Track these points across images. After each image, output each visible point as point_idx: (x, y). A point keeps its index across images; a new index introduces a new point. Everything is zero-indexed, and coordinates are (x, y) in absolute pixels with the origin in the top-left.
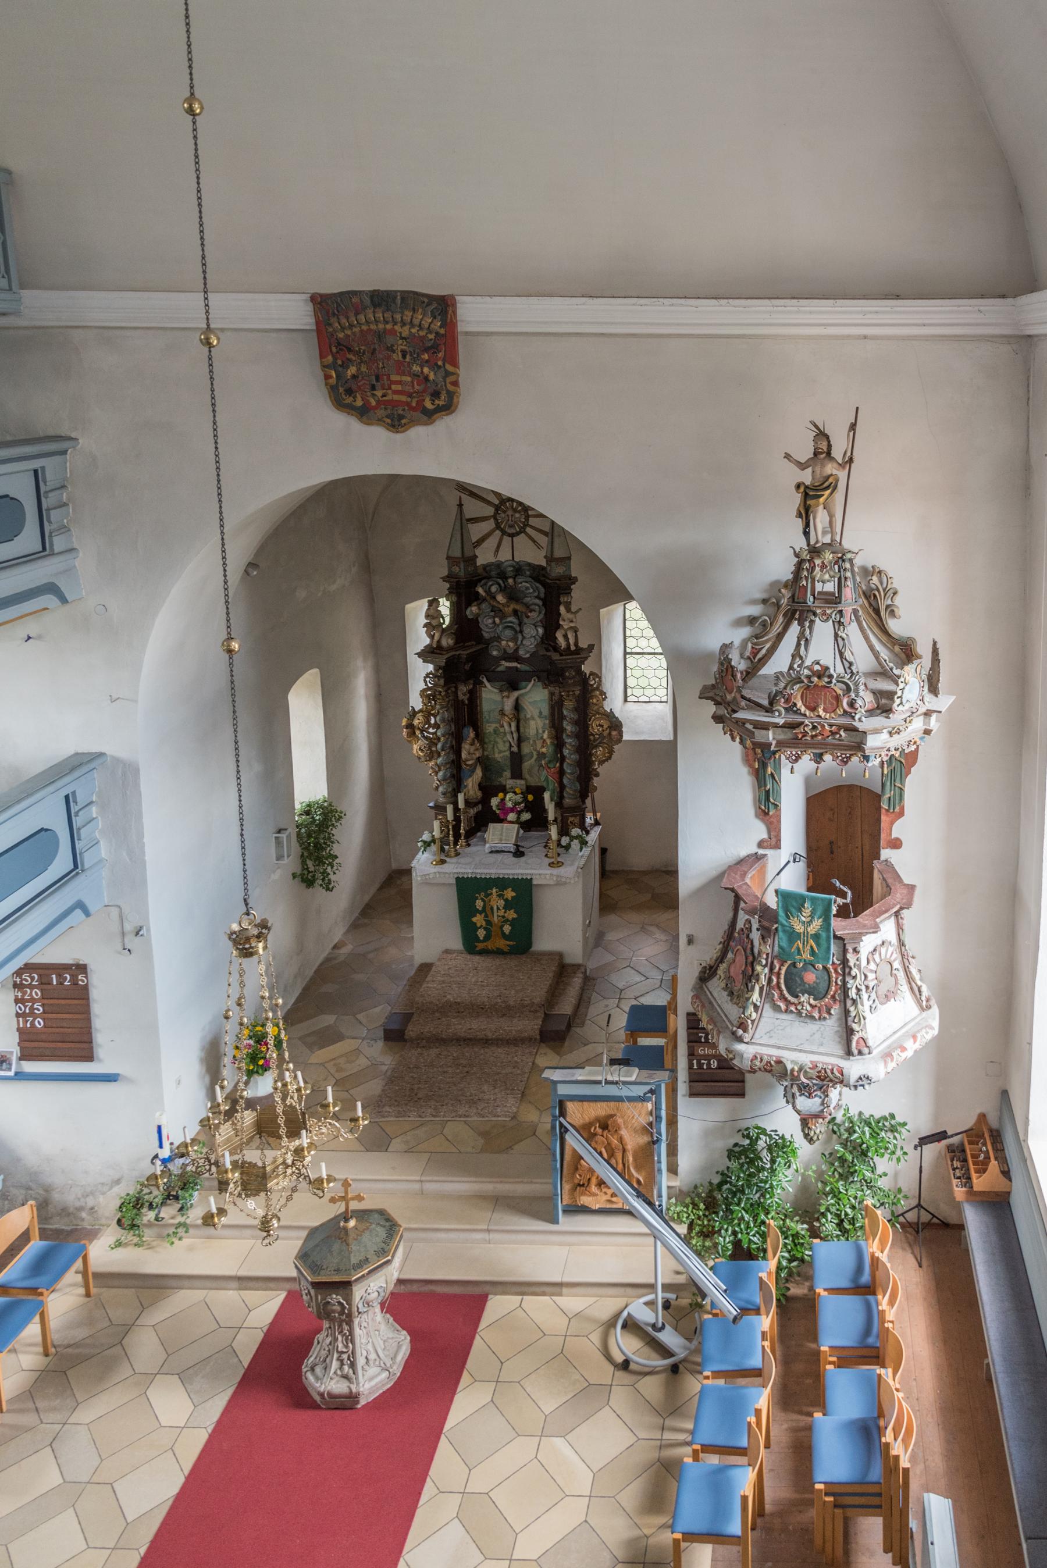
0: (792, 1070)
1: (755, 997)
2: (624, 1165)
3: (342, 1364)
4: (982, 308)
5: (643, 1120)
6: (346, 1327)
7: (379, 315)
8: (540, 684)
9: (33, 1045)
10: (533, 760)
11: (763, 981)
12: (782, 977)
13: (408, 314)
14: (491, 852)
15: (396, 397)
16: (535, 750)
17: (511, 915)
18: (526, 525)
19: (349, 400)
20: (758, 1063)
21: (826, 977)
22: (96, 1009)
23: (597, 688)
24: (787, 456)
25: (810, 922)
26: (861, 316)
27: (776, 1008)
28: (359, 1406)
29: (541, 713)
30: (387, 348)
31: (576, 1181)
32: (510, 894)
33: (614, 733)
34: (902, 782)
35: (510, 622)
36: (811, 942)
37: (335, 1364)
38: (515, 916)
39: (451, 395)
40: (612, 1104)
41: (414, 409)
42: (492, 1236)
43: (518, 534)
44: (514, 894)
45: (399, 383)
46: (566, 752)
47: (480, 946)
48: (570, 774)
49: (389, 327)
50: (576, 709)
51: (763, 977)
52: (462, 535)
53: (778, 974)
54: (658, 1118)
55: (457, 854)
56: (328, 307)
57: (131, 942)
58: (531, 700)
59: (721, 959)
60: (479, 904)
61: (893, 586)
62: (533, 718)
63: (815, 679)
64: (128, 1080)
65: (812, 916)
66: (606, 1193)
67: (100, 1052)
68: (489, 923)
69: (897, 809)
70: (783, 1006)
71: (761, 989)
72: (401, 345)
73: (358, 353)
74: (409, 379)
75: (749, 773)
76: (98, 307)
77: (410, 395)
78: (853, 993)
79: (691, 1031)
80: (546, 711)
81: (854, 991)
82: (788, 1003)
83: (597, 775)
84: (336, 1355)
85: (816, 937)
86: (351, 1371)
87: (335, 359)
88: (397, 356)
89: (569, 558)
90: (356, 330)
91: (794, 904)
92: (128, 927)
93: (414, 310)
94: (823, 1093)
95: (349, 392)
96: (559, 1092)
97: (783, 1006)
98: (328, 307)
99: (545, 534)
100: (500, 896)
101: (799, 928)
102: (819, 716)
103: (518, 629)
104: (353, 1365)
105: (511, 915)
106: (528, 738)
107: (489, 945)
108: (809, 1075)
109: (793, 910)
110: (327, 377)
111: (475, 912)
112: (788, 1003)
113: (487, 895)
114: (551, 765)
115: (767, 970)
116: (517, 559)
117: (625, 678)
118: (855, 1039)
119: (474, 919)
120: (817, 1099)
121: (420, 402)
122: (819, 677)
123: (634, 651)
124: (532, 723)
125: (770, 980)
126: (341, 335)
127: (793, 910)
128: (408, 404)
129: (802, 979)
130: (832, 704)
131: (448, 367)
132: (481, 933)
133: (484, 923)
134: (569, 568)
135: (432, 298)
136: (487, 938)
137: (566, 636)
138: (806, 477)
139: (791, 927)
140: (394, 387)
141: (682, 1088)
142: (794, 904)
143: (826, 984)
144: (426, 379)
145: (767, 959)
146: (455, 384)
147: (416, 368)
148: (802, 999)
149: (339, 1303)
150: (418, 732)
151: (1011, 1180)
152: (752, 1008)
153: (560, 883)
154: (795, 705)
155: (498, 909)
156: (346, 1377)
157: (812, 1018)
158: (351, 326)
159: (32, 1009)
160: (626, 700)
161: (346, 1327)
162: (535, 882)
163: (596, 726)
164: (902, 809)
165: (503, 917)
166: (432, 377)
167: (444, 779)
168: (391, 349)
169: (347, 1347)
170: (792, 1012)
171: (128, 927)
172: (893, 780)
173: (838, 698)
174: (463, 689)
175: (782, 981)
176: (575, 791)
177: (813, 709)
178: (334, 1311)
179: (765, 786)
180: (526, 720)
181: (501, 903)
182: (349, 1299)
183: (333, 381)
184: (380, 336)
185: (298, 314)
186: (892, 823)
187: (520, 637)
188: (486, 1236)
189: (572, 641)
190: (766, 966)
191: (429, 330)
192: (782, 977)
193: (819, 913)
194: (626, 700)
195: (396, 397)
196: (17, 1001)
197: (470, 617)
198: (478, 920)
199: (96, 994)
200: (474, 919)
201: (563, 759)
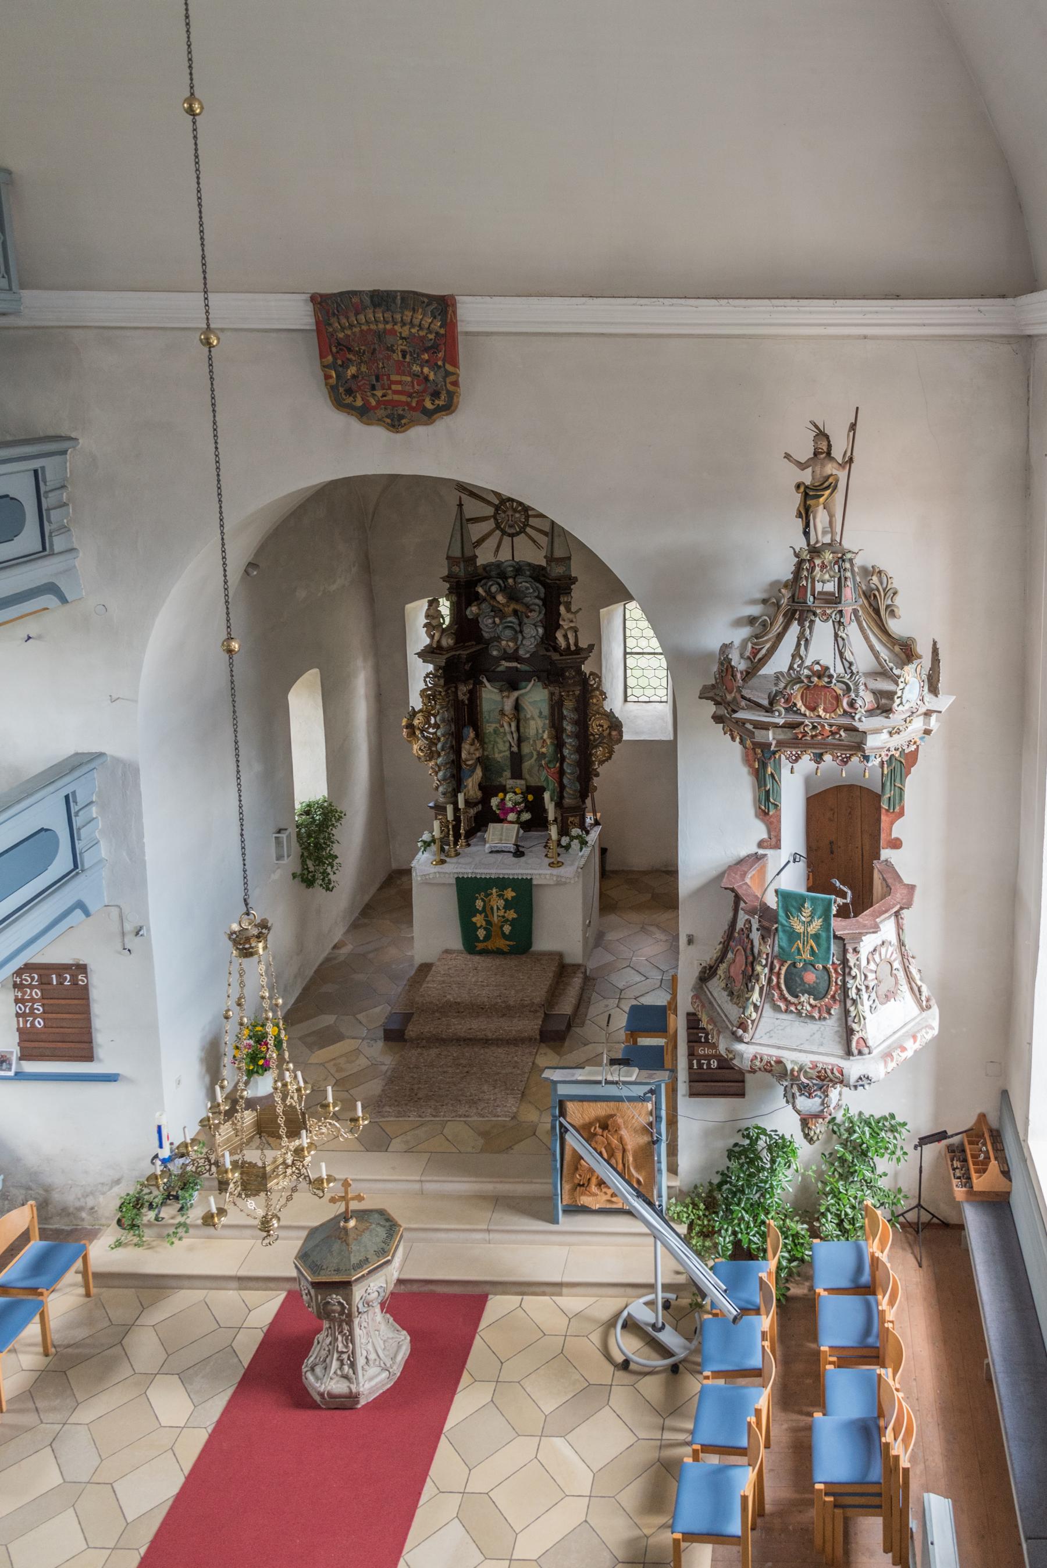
0: (792, 1070)
1: (755, 997)
2: (624, 1165)
3: (342, 1364)
4: (982, 308)
5: (643, 1120)
6: (346, 1327)
7: (379, 315)
8: (540, 684)
9: (33, 1045)
10: (533, 760)
11: (763, 981)
12: (782, 977)
13: (408, 314)
14: (491, 852)
15: (396, 397)
16: (535, 750)
17: (511, 915)
18: (526, 525)
19: (349, 400)
20: (758, 1063)
21: (826, 977)
22: (96, 1009)
23: (597, 688)
24: (787, 456)
25: (810, 922)
27: (776, 1008)
28: (359, 1406)
29: (541, 713)
30: (387, 348)
31: (576, 1181)
32: (510, 894)
34: (902, 782)
35: (510, 622)
36: (811, 942)
37: (335, 1364)
38: (515, 916)
39: (451, 395)
40: (612, 1104)
41: (414, 409)
42: (492, 1236)
43: (518, 534)
44: (514, 894)
45: (399, 383)
46: (566, 752)
47: (480, 946)
48: (570, 774)
49: (389, 327)
50: (576, 709)
51: (763, 977)
52: (462, 535)
53: (778, 974)
54: (658, 1118)
55: (457, 854)
56: (328, 307)
57: (131, 942)
58: (531, 700)
59: (721, 959)
60: (479, 904)
61: (893, 586)
62: (533, 718)
63: (815, 679)
64: (128, 1080)
65: (812, 916)
66: (606, 1193)
67: (100, 1052)
68: (489, 923)
69: (897, 809)
70: (783, 1006)
71: (761, 989)
72: (401, 345)
73: (358, 353)
74: (409, 379)
75: (749, 773)
76: (98, 307)
77: (410, 395)
78: (853, 993)
79: (691, 1031)
80: (546, 711)
81: (854, 991)
82: (788, 1003)
83: (597, 775)
84: (336, 1355)
85: (816, 937)
86: (351, 1371)
87: (335, 359)
88: (397, 356)
89: (569, 558)
90: (356, 330)
91: (794, 904)
92: (128, 927)
93: (414, 310)
94: (823, 1093)
95: (349, 392)
96: (559, 1092)
97: (783, 1006)
98: (328, 307)
99: (545, 534)
100: (500, 896)
101: (799, 928)
102: (819, 716)
103: (518, 629)
104: (353, 1365)
105: (511, 915)
106: (528, 738)
107: (489, 945)
108: (809, 1075)
109: (793, 910)
110: (327, 377)
111: (475, 912)
112: (788, 1003)
113: (487, 895)
114: (551, 765)
115: (767, 970)
116: (517, 559)
117: (625, 678)
118: (855, 1039)
119: (474, 919)
120: (817, 1099)
121: (420, 402)
122: (819, 677)
123: (634, 651)
124: (532, 723)
125: (770, 980)
126: (341, 335)
127: (793, 910)
128: (408, 404)
129: (802, 979)
130: (832, 704)
131: (448, 367)
132: (481, 933)
133: (484, 923)
134: (569, 568)
135: (432, 298)
136: (487, 938)
137: (566, 636)
138: (806, 477)
139: (791, 927)
140: (394, 387)
141: (682, 1088)
142: (794, 904)
143: (826, 984)
144: (426, 379)
146: (455, 384)
147: (416, 368)
148: (802, 999)
149: (339, 1303)
150: (418, 732)
151: (1011, 1180)
152: (752, 1008)
153: (560, 883)
154: (795, 705)
155: (498, 909)
156: (346, 1377)
157: (812, 1018)
158: (351, 326)
159: (32, 1009)
160: (626, 700)
161: (346, 1327)
162: (535, 882)
163: (596, 726)
164: (902, 809)
165: (503, 917)
166: (432, 377)
167: (444, 779)
168: (391, 349)
169: (347, 1347)
170: (792, 1012)
171: (128, 927)
172: (893, 780)
174: (463, 689)
175: (782, 981)
176: (575, 791)
177: (813, 709)
178: (334, 1311)
179: (765, 786)
180: (526, 720)
181: (501, 903)
182: (349, 1299)
183: (333, 381)
184: (380, 336)
185: (298, 314)
186: (892, 823)
187: (520, 637)
188: (486, 1236)
189: (572, 641)
191: (429, 330)
192: (782, 977)
193: (819, 913)
194: (626, 700)
195: (396, 397)
196: (17, 1001)
197: (470, 617)
198: (478, 920)
199: (96, 994)
200: (474, 919)
201: (563, 759)
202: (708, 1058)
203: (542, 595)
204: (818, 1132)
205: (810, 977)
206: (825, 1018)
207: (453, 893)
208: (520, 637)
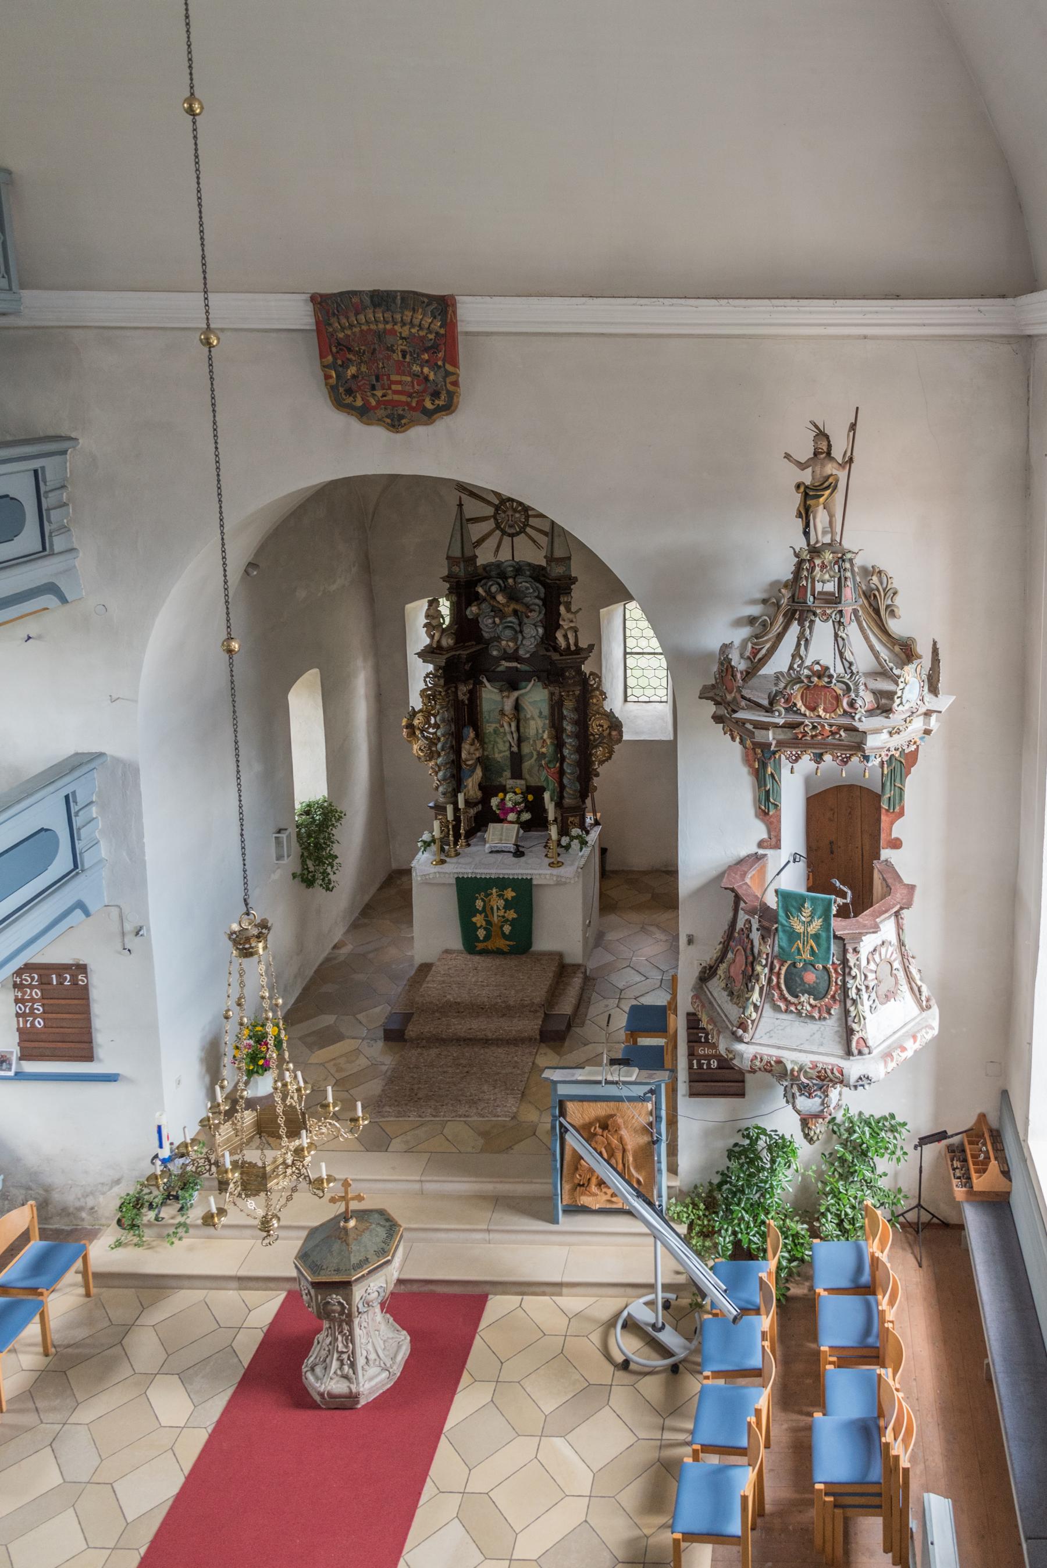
0: (792, 1070)
1: (755, 997)
2: (624, 1165)
3: (342, 1364)
4: (982, 308)
5: (643, 1120)
6: (346, 1327)
7: (379, 315)
9: (33, 1045)
10: (533, 760)
11: (763, 981)
12: (782, 977)
13: (408, 314)
14: (491, 852)
15: (396, 397)
16: (535, 750)
17: (511, 915)
18: (526, 525)
19: (349, 400)
20: (758, 1063)
21: (826, 977)
22: (96, 1009)
23: (597, 688)
24: (787, 456)
25: (810, 922)
26: (861, 316)
28: (359, 1406)
29: (541, 713)
30: (387, 348)
31: (576, 1181)
32: (510, 894)
33: (614, 733)
34: (902, 782)
35: (510, 622)
36: (811, 942)
38: (515, 916)
39: (451, 395)
40: (612, 1104)
41: (414, 409)
42: (492, 1236)
43: (518, 534)
44: (514, 894)
45: (399, 383)
46: (566, 752)
47: (480, 946)
48: (570, 774)
49: (389, 327)
50: (576, 709)
51: (763, 977)
52: (462, 535)
53: (778, 974)
54: (658, 1118)
55: (457, 854)
56: (328, 307)
57: (131, 942)
58: (531, 700)
59: (721, 959)
60: (479, 904)
61: (893, 586)
62: (533, 718)
63: (815, 679)
64: (128, 1080)
65: (812, 916)
66: (606, 1193)
67: (100, 1052)
68: (489, 923)
70: (783, 1006)
71: (761, 989)
72: (401, 345)
73: (358, 353)
74: (409, 379)
75: (749, 773)
76: (98, 307)
77: (410, 395)
78: (853, 993)
79: (691, 1031)
80: (546, 711)
81: (854, 991)
82: (788, 1003)
83: (597, 775)
84: (336, 1355)
85: (816, 937)
86: (351, 1371)
87: (335, 359)
88: (397, 356)
89: (569, 558)
90: (356, 330)
91: (794, 904)
92: (128, 927)
93: (414, 310)
95: (349, 392)
96: (559, 1092)
97: (783, 1006)
98: (328, 307)
99: (545, 534)
100: (500, 896)
101: (799, 928)
103: (518, 629)
104: (353, 1365)
106: (528, 738)
107: (489, 945)
109: (793, 910)
110: (327, 377)
111: (475, 912)
112: (788, 1003)
113: (487, 895)
114: (551, 765)
115: (767, 970)
116: (517, 559)
117: (625, 678)
118: (855, 1039)
119: (474, 919)
120: (817, 1099)
121: (420, 402)
122: (819, 677)
123: (634, 651)
124: (532, 723)
125: (770, 980)
126: (341, 335)
127: (793, 910)
128: (408, 404)
129: (802, 979)
130: (832, 704)
131: (448, 367)
132: (481, 933)
133: (484, 923)
134: (569, 568)
135: (432, 298)
136: (487, 938)
137: (566, 636)
138: (806, 477)
139: (791, 927)
140: (394, 387)
141: (682, 1088)
142: (794, 904)
143: (826, 984)
144: (426, 379)
145: (767, 959)
146: (455, 384)
147: (416, 368)
149: (339, 1303)
150: (418, 732)
151: (1011, 1180)
152: (752, 1008)
153: (560, 883)
155: (498, 909)
157: (812, 1018)
158: (351, 326)
159: (32, 1009)
160: (626, 700)
161: (346, 1327)
162: (535, 882)
163: (596, 726)
164: (902, 809)
165: (503, 917)
166: (432, 377)
168: (391, 349)
169: (347, 1347)
170: (792, 1012)
171: (128, 927)
172: (893, 780)
173: (838, 698)
174: (463, 689)
175: (782, 981)
176: (575, 791)
177: (813, 709)
178: (334, 1311)
179: (765, 786)
180: (526, 720)
181: (501, 903)
182: (349, 1299)
183: (333, 381)
184: (380, 336)
185: (298, 314)
186: (892, 823)
187: (520, 637)
188: (486, 1236)
189: (572, 641)
190: (766, 966)
191: (429, 330)
192: (782, 977)
193: (819, 913)
194: (626, 700)
195: (396, 397)
196: (17, 1001)
197: (470, 617)
198: (478, 920)
199: (96, 994)
200: (474, 919)
201: (563, 759)
202: (708, 1058)
203: (542, 595)
204: (818, 1132)
205: (810, 977)
206: (825, 1018)
207: (453, 893)
208: (520, 637)
